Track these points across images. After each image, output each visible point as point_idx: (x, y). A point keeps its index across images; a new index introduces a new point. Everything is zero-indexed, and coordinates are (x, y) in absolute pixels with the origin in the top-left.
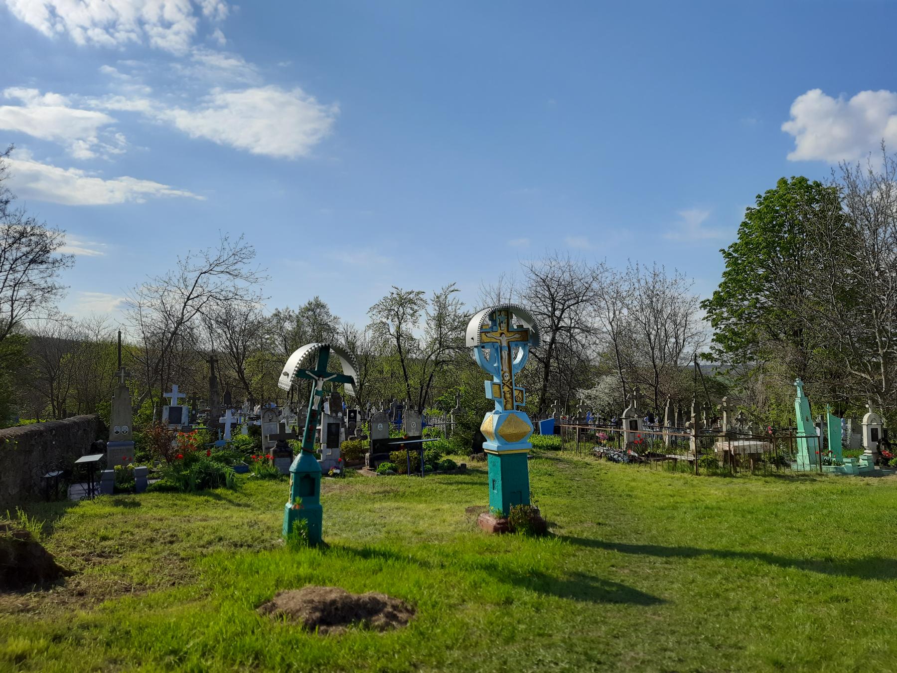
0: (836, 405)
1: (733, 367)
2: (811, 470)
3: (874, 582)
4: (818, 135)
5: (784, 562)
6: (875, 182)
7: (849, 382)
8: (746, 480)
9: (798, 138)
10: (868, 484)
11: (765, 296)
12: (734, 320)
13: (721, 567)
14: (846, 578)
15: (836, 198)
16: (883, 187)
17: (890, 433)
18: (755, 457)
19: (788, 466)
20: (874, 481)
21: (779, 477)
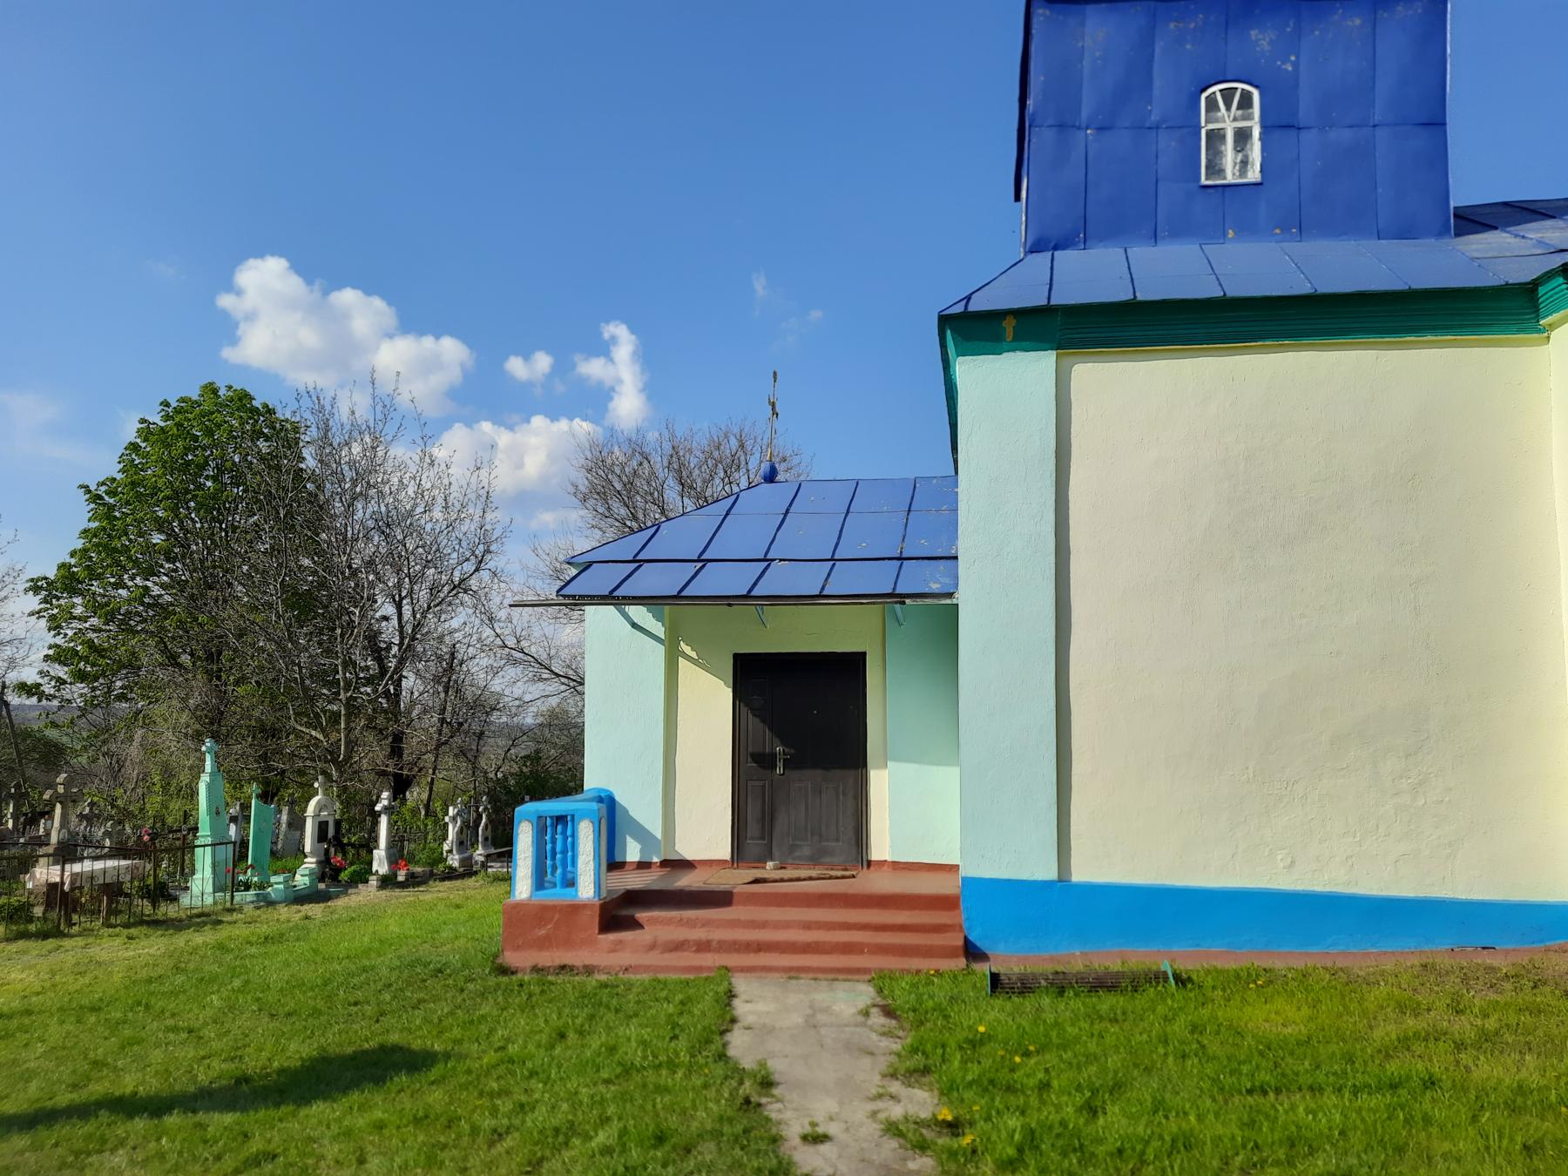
0: (266, 783)
1: (83, 712)
2: (215, 903)
3: (318, 1108)
4: (281, 331)
5: (156, 1107)
6: (356, 430)
7: (290, 745)
8: (91, 940)
9: (242, 326)
10: (307, 918)
11: (163, 586)
12: (94, 621)
13: (22, 1152)
14: (272, 1113)
15: (297, 441)
16: (367, 439)
17: (345, 825)
18: (112, 890)
19: (175, 899)
20: (315, 910)
21: (155, 923)
